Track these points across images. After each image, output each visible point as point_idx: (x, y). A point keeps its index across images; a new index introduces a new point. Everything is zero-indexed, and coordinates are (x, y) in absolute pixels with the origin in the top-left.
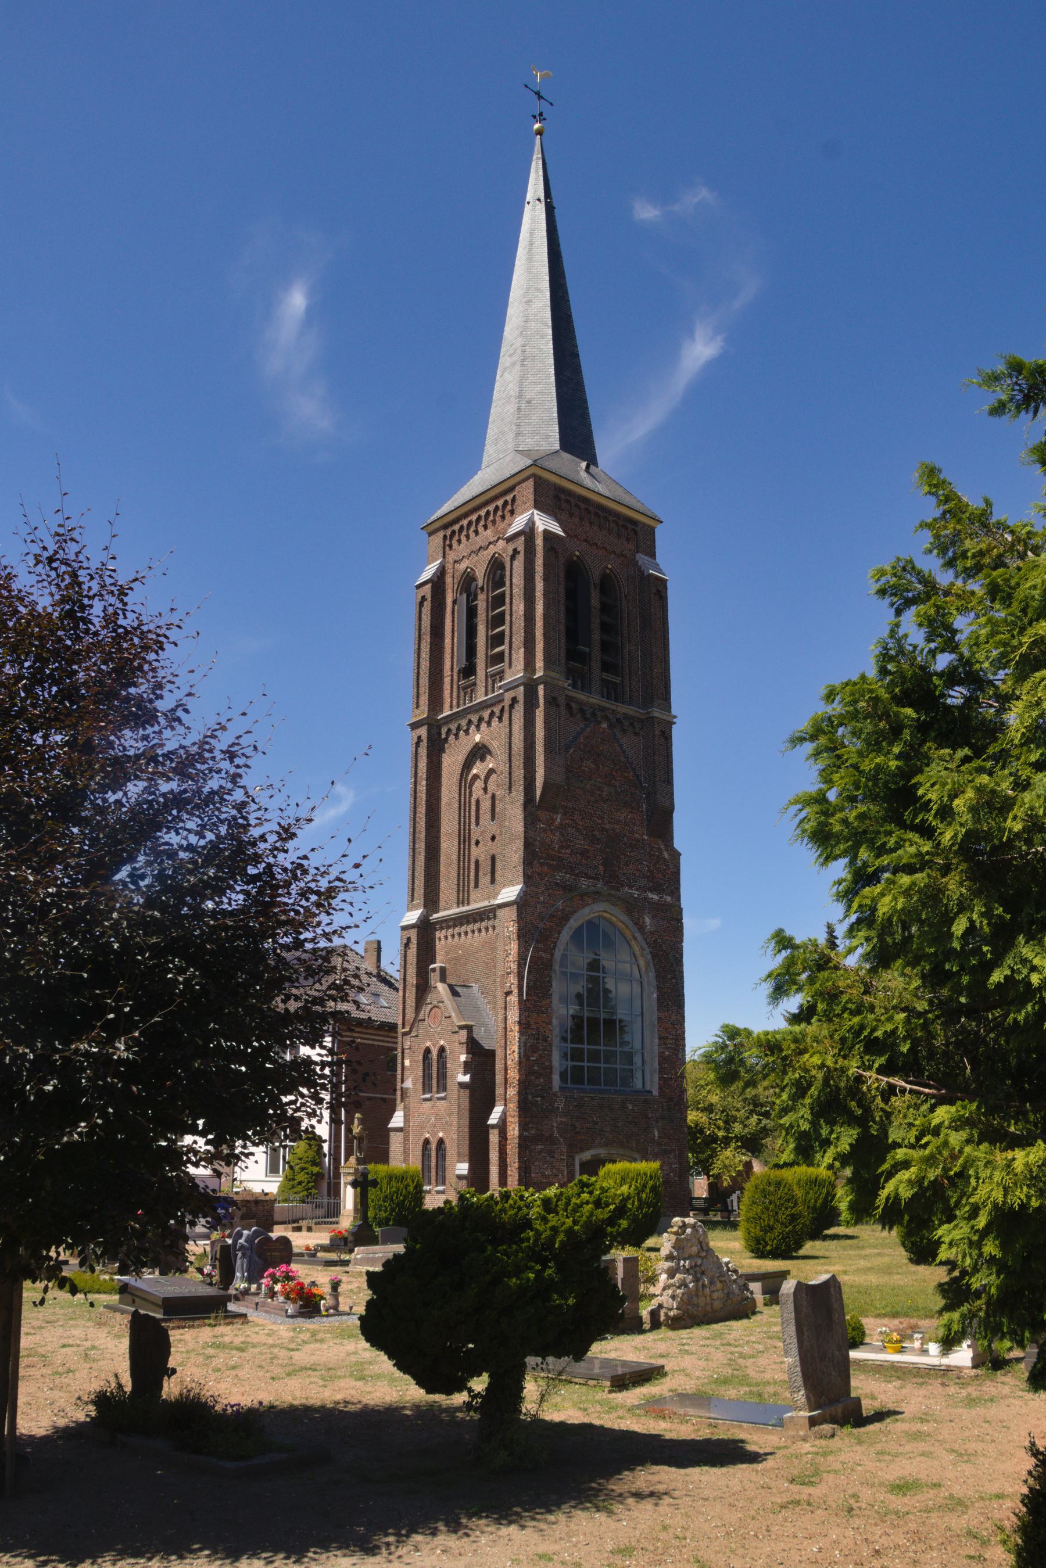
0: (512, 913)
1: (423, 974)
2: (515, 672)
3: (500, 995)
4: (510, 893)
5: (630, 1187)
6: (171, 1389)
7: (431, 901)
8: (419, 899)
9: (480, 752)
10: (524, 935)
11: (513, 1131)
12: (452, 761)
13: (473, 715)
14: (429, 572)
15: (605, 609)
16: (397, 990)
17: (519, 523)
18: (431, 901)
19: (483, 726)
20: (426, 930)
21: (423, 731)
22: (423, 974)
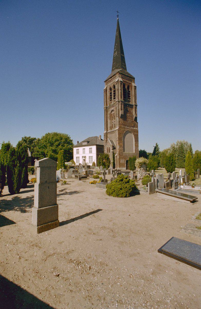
0: (117, 131)
1: (107, 139)
2: (117, 100)
3: (116, 141)
4: (117, 128)
5: (167, 181)
6: (9, 193)
7: (107, 130)
8: (106, 130)
9: (113, 110)
10: (119, 134)
11: (118, 157)
12: (109, 112)
13: (110, 107)
14: (105, 88)
15: (108, 151)
16: (104, 107)
17: (117, 80)
18: (107, 130)
19: (113, 107)
20: (107, 133)
21: (105, 108)
22: (107, 139)
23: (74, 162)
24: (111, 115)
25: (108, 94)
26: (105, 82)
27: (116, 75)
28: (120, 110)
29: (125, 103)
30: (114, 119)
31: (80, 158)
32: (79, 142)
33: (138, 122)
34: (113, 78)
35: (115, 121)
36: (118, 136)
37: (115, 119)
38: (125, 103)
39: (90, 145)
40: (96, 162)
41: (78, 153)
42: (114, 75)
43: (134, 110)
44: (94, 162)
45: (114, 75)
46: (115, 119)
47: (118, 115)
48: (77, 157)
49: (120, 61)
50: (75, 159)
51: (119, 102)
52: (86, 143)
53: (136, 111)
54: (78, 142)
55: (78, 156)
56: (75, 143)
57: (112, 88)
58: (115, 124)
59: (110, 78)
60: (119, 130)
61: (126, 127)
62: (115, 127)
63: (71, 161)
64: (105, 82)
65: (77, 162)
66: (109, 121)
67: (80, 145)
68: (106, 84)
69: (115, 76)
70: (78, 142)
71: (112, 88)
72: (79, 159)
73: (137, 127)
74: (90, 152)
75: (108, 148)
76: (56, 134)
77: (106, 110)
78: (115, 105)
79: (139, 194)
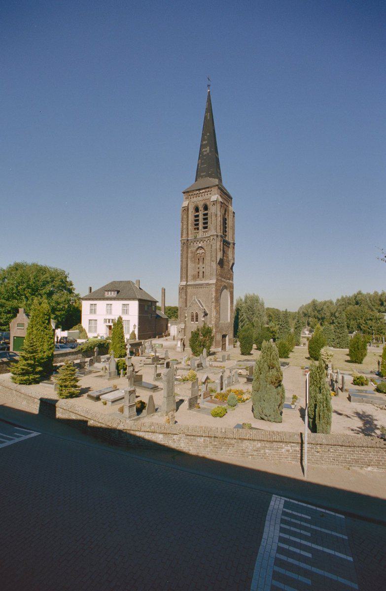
0: (214, 286)
13: (196, 240)
23: (82, 331)
24: (194, 254)
25: (191, 218)
26: (184, 193)
27: (212, 189)
28: (218, 250)
29: (211, 233)
30: (201, 263)
31: (98, 322)
32: (92, 291)
33: (233, 271)
34: (204, 191)
35: (204, 266)
36: (214, 294)
37: (203, 263)
38: (211, 233)
39: (126, 299)
40: (136, 333)
41: (93, 311)
42: (208, 188)
43: (230, 250)
44: (133, 332)
45: (208, 188)
46: (203, 263)
47: (214, 259)
48: (90, 320)
49: (210, 165)
50: (85, 323)
51: (217, 236)
52: (218, 308)
53: (233, 253)
54: (91, 289)
55: (93, 317)
56: (80, 289)
57: (201, 208)
58: (203, 272)
59: (197, 190)
60: (216, 284)
61: (223, 279)
62: (203, 277)
63: (77, 326)
64: (184, 193)
65: (90, 331)
66: (191, 265)
67: (97, 296)
68: (187, 198)
69: (210, 189)
70: (91, 289)
71: (201, 208)
72: (96, 324)
73: (232, 280)
74: (91, 312)
75: (194, 313)
76: (42, 270)
77: (186, 244)
78: (206, 239)
79: (42, 400)
